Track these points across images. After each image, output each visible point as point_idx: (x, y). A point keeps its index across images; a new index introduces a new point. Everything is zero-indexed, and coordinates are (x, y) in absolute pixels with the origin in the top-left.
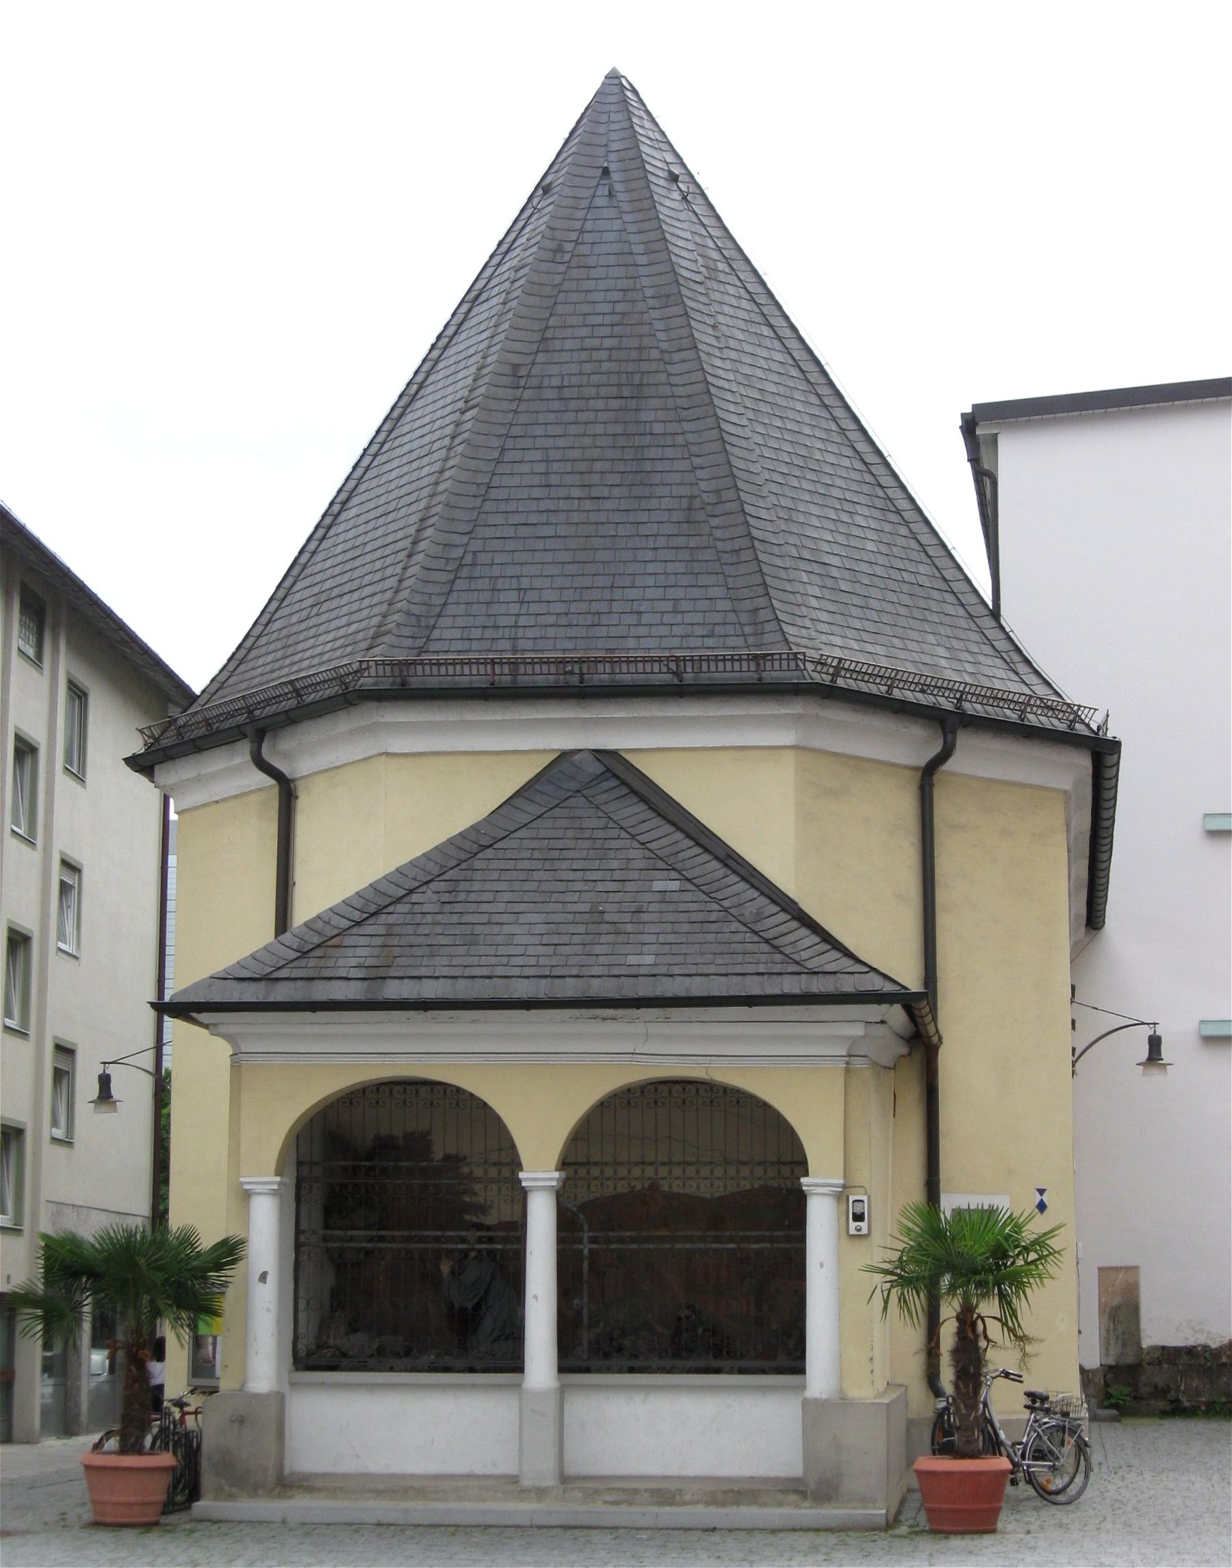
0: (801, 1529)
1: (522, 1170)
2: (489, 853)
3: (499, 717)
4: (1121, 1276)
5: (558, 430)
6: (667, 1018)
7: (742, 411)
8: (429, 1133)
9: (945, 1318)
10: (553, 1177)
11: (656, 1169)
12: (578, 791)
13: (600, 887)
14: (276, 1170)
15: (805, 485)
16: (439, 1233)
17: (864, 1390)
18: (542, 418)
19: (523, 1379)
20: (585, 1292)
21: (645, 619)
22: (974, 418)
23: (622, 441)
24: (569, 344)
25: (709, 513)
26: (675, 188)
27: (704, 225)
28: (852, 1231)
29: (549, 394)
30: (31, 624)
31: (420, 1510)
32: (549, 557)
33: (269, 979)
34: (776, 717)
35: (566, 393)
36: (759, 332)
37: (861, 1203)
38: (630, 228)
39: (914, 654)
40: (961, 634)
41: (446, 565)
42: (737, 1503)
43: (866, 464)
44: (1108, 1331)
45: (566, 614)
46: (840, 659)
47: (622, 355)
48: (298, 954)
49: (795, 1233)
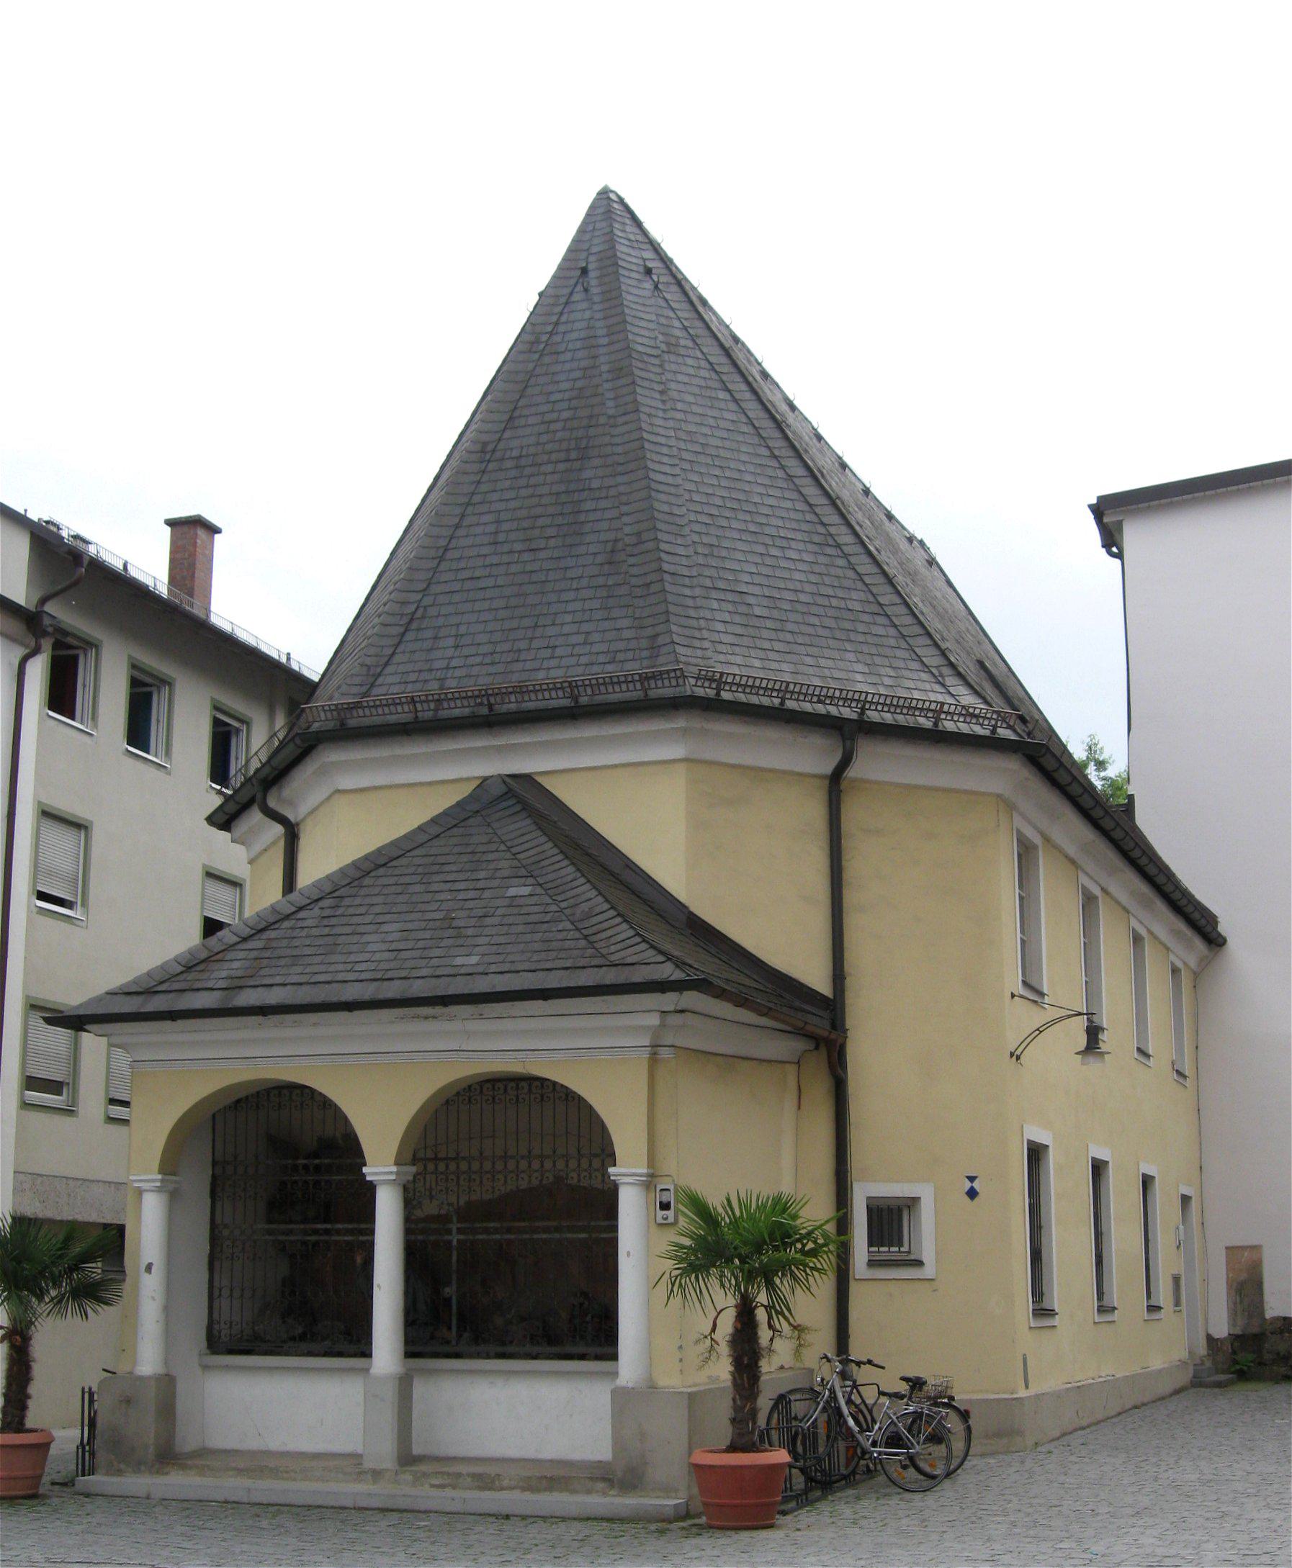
0: (595, 1519)
2: (381, 871)
4: (1246, 1254)
5: (512, 494)
6: (481, 1015)
7: (677, 462)
9: (721, 1308)
12: (478, 812)
13: (462, 896)
15: (735, 524)
17: (670, 1380)
18: (500, 485)
19: (371, 1364)
20: (454, 1282)
21: (559, 652)
22: (1099, 508)
23: (564, 498)
24: (531, 420)
25: (628, 553)
27: (673, 309)
28: (660, 1220)
29: (509, 464)
31: (266, 1488)
32: (486, 605)
33: (150, 992)
35: (523, 462)
37: (668, 1192)
38: (599, 315)
39: (826, 670)
40: (888, 652)
41: (400, 620)
42: (549, 1489)
44: (1235, 1304)
45: (492, 654)
47: (575, 424)
48: (184, 969)
49: (363, 1226)
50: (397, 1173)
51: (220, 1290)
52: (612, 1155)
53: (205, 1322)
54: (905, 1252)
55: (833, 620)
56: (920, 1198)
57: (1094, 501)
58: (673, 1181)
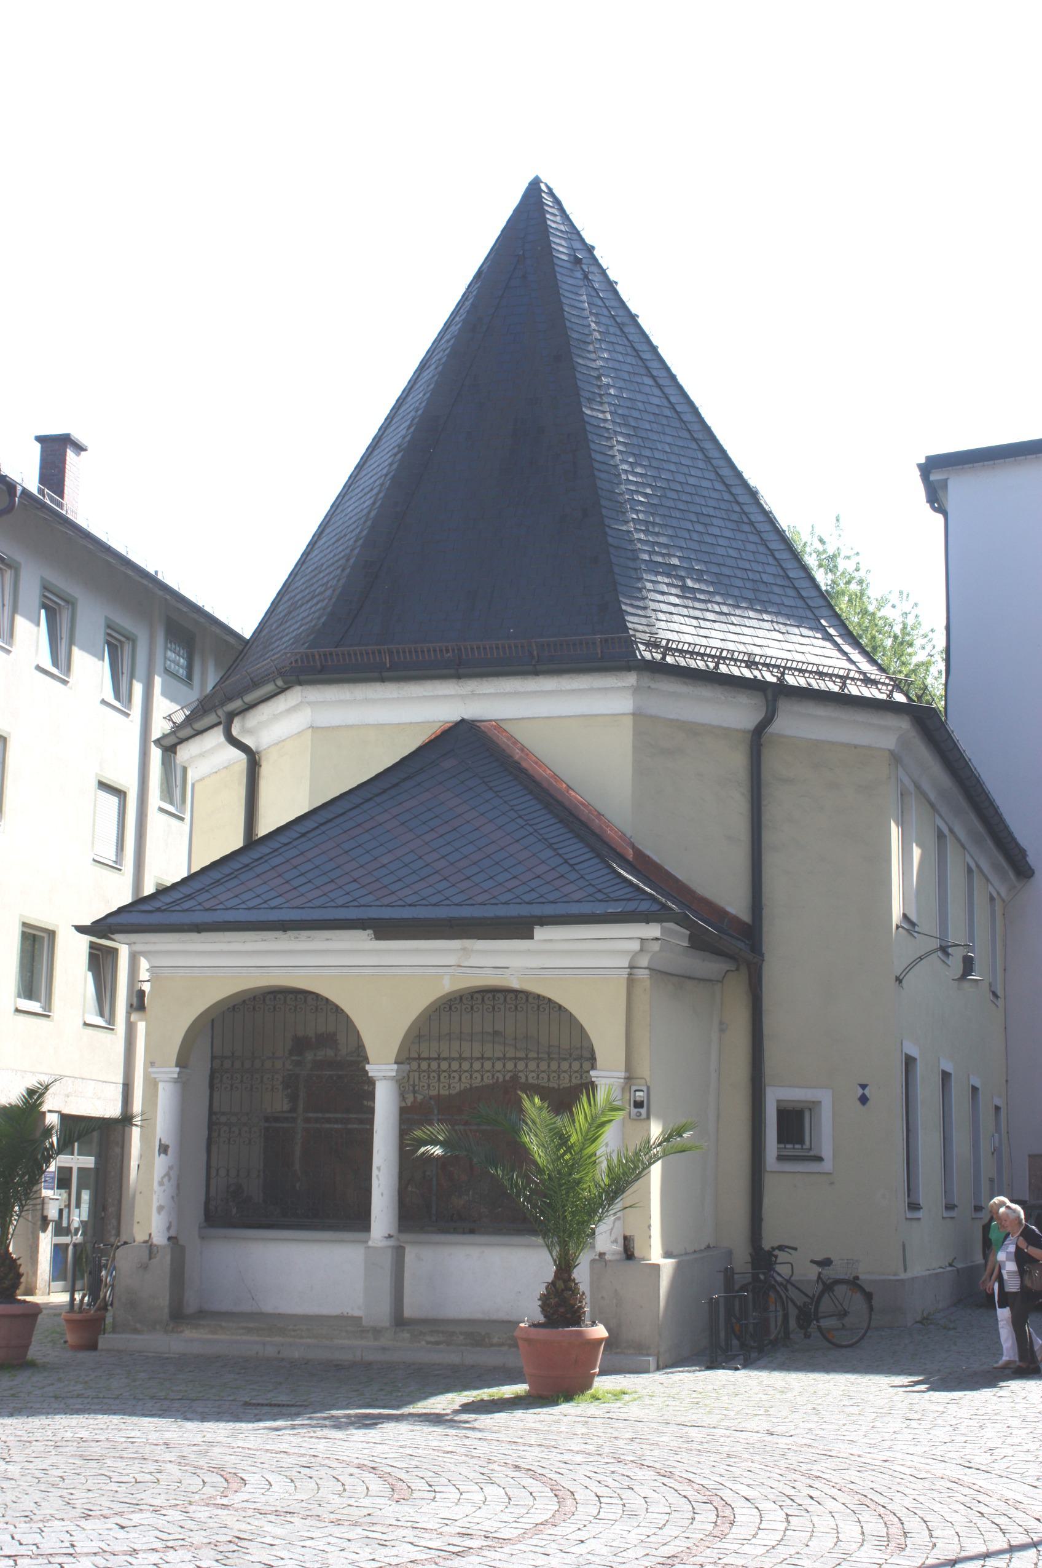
1: (368, 1063)
3: (395, 695)
8: (335, 1034)
10: (391, 1069)
11: (493, 1064)
14: (176, 1062)
16: (320, 1115)
19: (370, 1235)
26: (579, 269)
30: (182, 652)
34: (592, 690)
36: (640, 381)
43: (726, 485)
46: (668, 641)
50: (397, 1071)
51: (218, 1170)
52: (592, 1059)
53: (203, 1198)
54: (806, 1149)
55: (752, 591)
56: (820, 1102)
57: (923, 461)
58: (646, 1082)
